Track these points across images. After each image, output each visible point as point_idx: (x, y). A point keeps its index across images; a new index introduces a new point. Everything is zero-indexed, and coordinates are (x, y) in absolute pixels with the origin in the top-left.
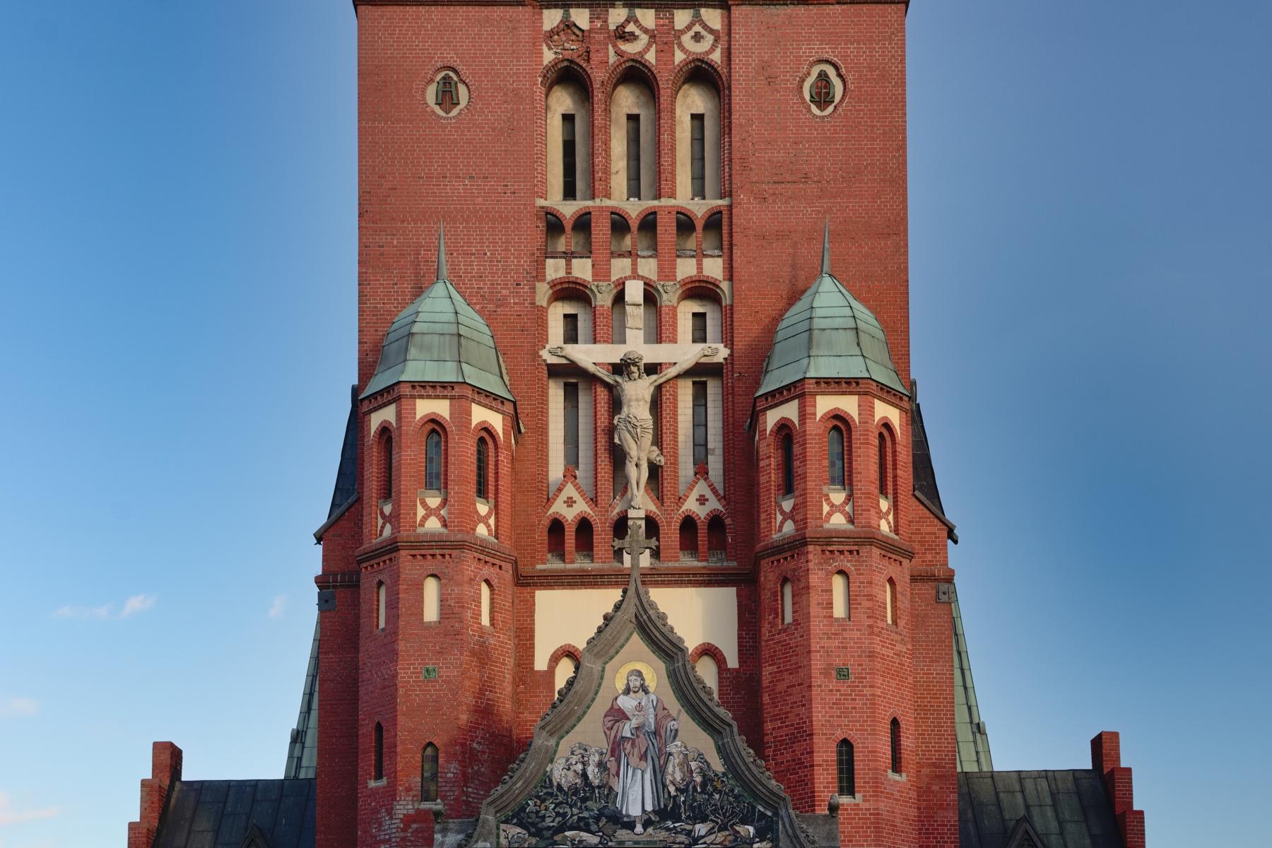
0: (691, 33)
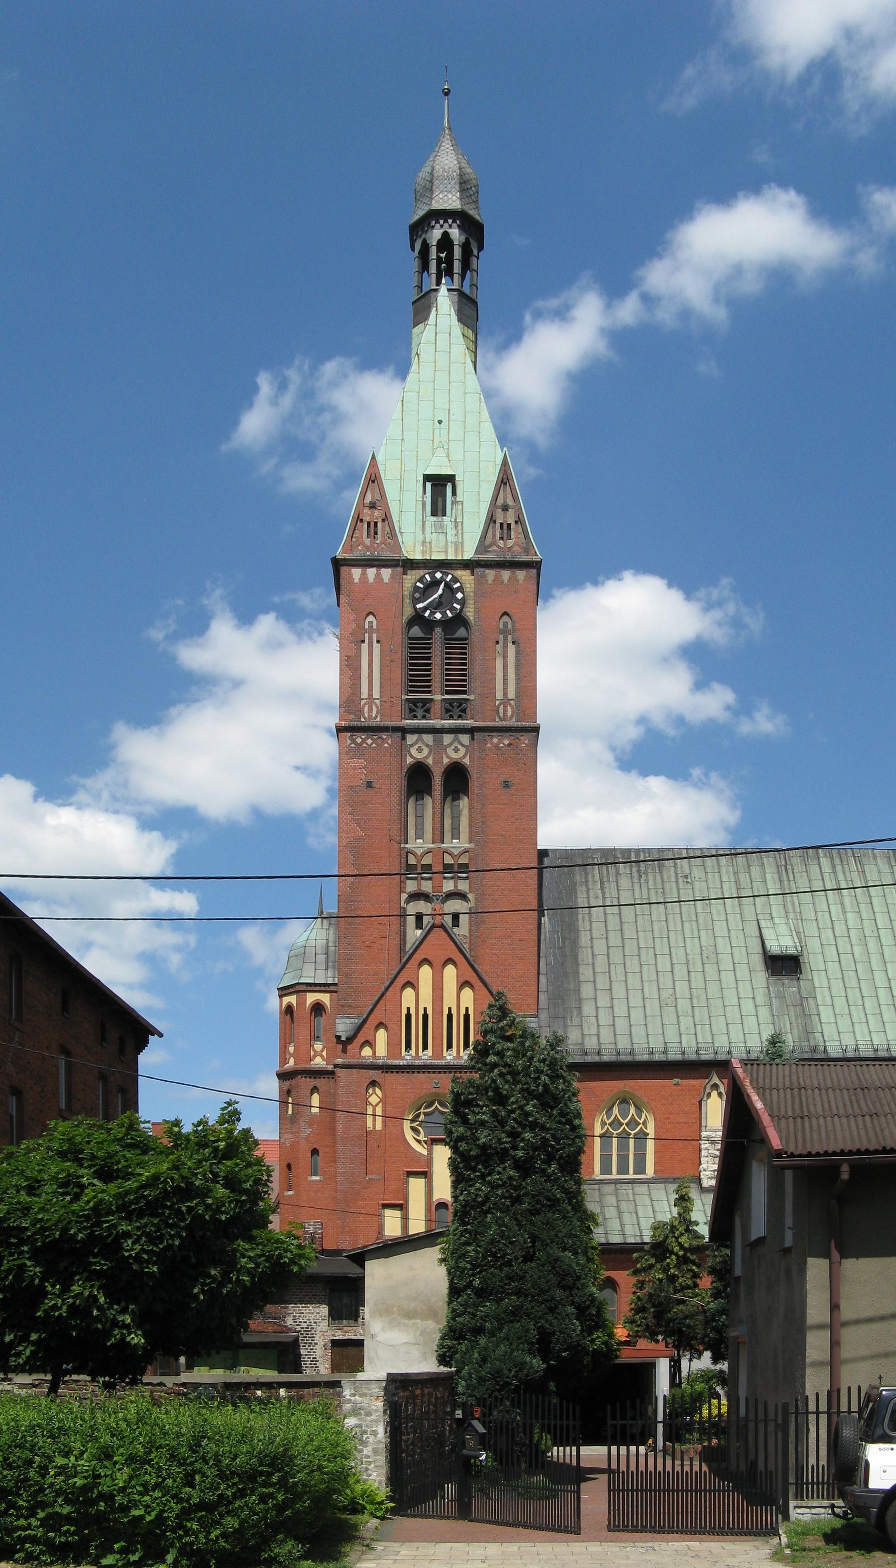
0: (416, 747)
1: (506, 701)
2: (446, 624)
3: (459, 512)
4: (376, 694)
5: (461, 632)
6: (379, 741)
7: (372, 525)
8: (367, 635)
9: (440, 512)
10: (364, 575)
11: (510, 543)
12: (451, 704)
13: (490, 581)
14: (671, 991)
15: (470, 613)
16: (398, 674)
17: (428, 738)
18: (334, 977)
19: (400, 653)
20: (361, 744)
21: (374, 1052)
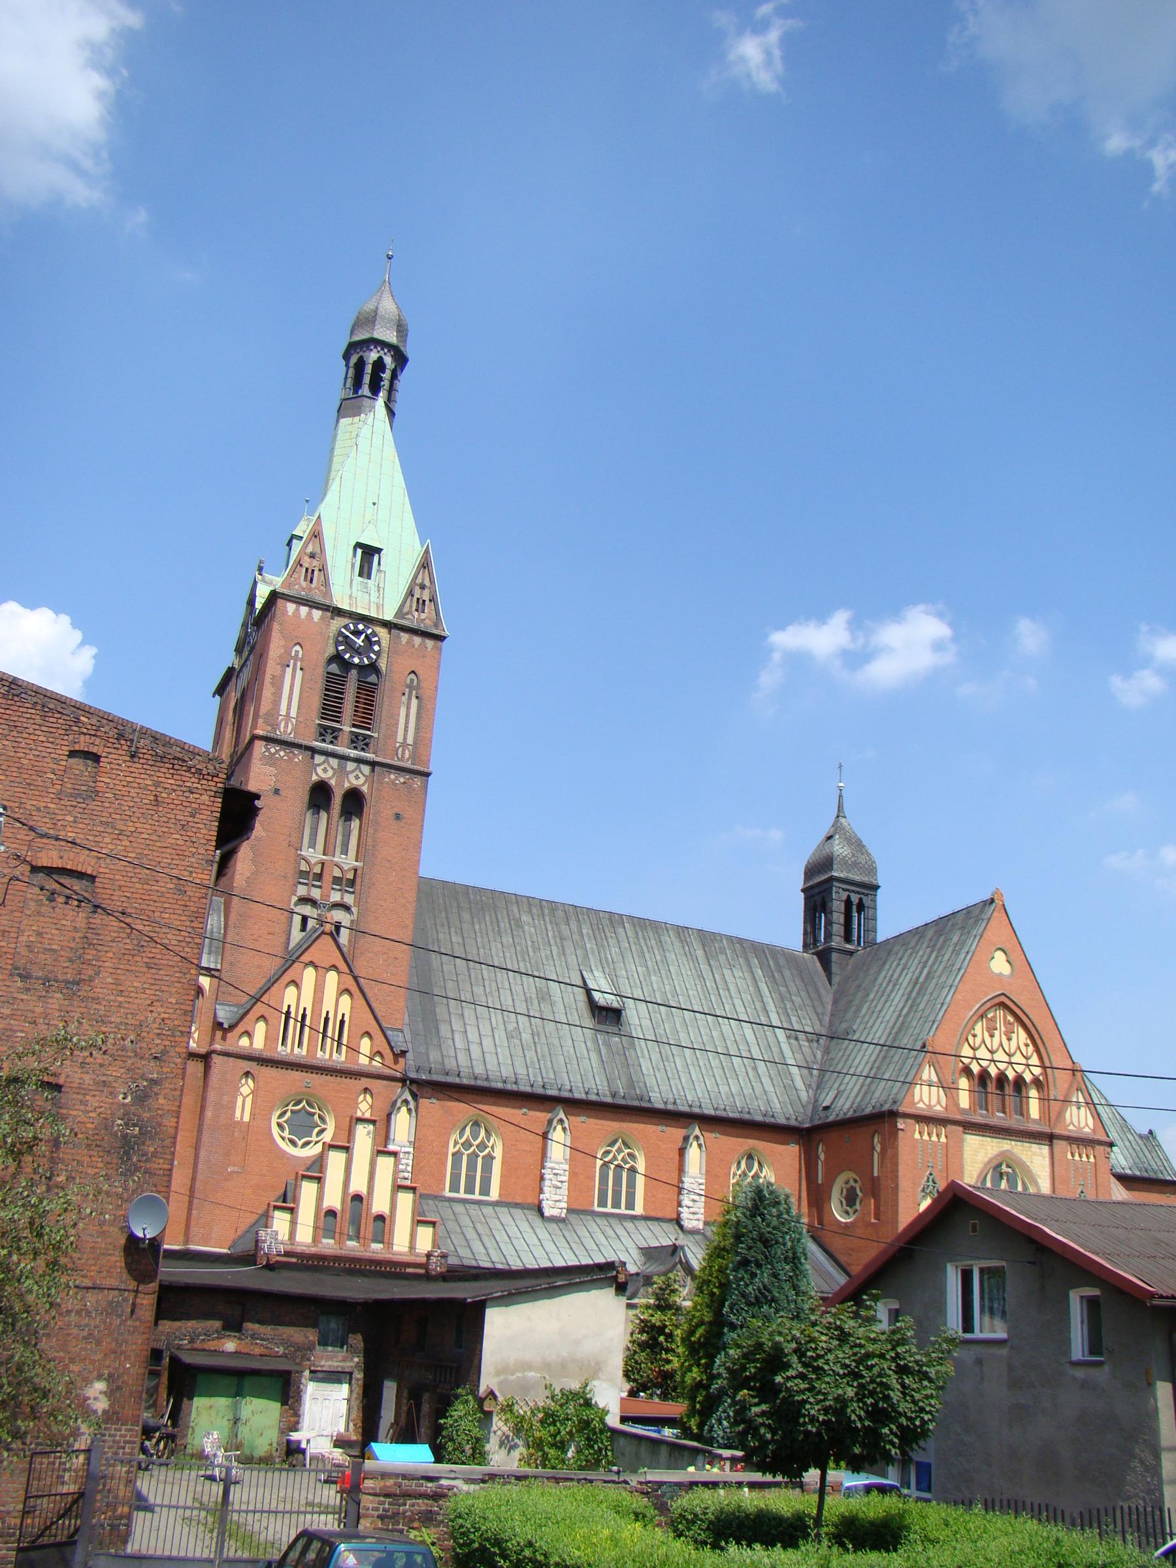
1: (404, 745)
2: (361, 668)
3: (382, 579)
4: (293, 713)
5: (373, 678)
6: (291, 755)
7: (310, 571)
8: (292, 661)
9: (365, 575)
11: (423, 616)
12: (356, 737)
13: (404, 643)
14: (515, 1025)
15: (382, 665)
16: (316, 701)
17: (334, 762)
18: (217, 963)
19: (319, 684)
20: (274, 754)
21: (251, 1044)
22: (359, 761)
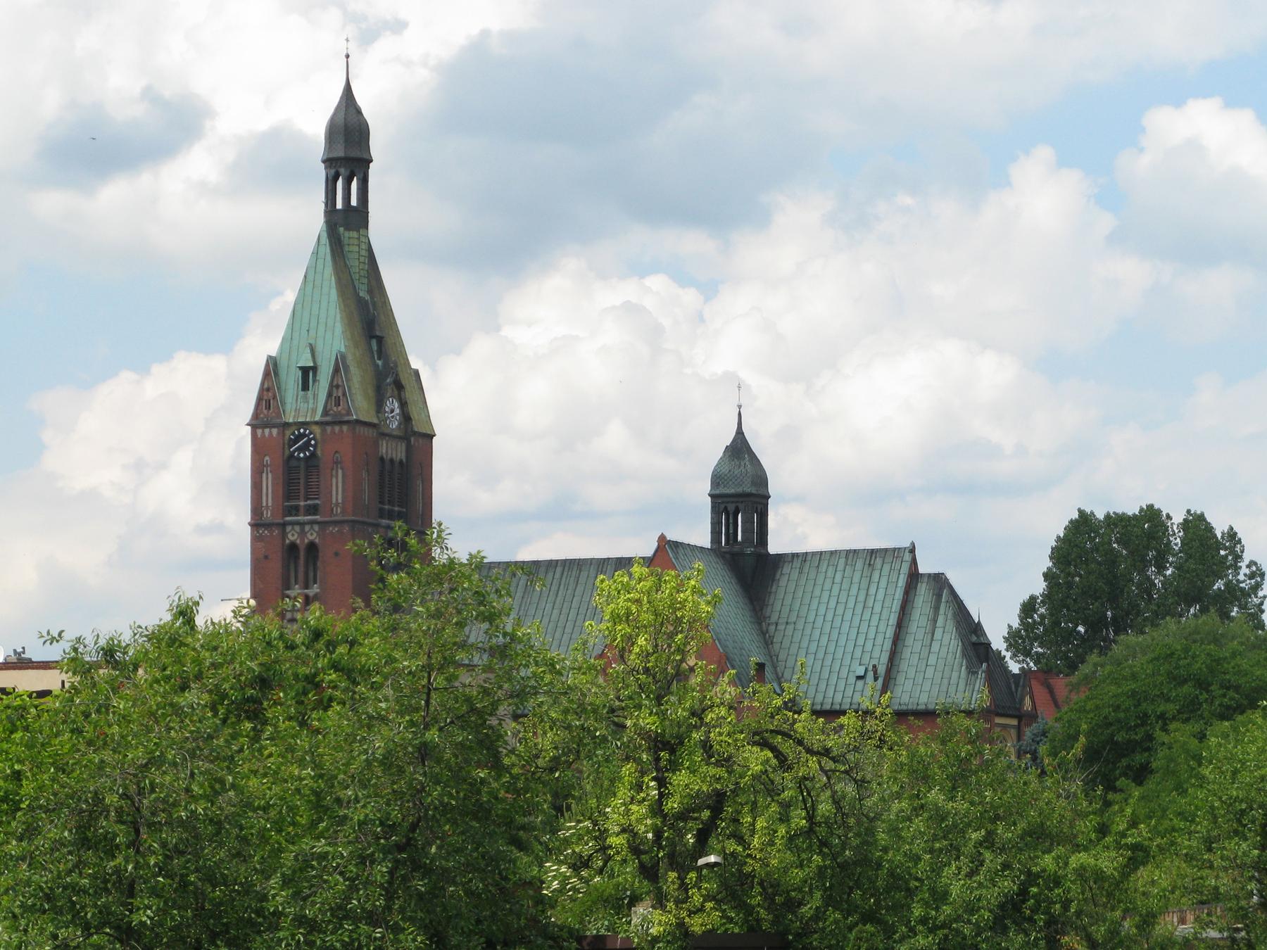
1: (337, 504)
4: (270, 504)
10: (271, 433)
11: (340, 408)
15: (319, 453)
22: (312, 523)
